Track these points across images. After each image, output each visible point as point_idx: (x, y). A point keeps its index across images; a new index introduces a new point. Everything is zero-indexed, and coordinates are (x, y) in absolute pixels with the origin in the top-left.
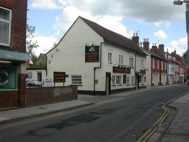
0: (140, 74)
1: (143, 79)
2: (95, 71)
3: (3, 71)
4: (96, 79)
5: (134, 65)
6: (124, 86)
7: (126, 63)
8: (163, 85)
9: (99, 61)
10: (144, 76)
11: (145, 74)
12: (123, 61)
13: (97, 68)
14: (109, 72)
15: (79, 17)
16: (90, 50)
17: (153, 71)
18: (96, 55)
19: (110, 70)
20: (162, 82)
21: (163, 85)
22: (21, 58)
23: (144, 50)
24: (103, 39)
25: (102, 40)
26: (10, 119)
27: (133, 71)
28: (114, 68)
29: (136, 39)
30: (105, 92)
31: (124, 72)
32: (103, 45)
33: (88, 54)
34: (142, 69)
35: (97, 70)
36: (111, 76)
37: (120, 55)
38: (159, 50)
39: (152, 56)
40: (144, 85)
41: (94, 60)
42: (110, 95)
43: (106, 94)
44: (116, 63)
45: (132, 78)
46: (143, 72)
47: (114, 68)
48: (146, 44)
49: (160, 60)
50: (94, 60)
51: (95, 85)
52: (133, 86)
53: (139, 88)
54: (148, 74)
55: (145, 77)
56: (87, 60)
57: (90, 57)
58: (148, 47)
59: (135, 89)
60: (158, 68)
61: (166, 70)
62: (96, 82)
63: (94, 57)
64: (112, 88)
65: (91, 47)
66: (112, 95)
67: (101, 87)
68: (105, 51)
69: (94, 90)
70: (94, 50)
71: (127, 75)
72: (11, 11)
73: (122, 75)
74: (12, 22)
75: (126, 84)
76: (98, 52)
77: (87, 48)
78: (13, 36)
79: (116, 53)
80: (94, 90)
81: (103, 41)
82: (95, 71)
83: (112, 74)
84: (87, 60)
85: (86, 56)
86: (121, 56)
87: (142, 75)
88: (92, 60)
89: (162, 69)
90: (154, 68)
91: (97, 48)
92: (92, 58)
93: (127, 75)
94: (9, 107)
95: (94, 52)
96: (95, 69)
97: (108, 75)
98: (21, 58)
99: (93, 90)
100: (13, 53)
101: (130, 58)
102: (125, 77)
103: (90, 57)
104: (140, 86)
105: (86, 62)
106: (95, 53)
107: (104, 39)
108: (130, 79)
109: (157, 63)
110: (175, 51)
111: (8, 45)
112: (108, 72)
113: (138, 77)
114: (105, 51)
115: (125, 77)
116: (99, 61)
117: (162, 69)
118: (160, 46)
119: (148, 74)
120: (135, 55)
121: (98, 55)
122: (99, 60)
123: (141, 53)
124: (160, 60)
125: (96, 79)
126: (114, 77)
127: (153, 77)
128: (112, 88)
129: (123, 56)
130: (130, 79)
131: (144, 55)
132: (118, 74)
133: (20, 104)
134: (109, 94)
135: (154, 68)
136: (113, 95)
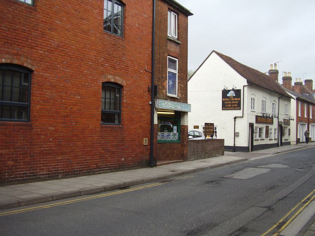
0: (283, 126)
1: (286, 131)
2: (235, 121)
3: (168, 123)
4: (236, 131)
5: (277, 112)
6: (267, 142)
7: (269, 111)
8: (312, 142)
9: (240, 109)
10: (288, 128)
11: (289, 125)
12: (266, 108)
13: (238, 117)
14: (252, 122)
15: (213, 51)
16: (228, 95)
17: (299, 120)
18: (236, 101)
19: (253, 121)
20: (310, 137)
21: (312, 142)
22: (186, 109)
23: (288, 92)
24: (246, 80)
25: (244, 82)
26: (108, 184)
27: (275, 121)
28: (257, 117)
29: (275, 73)
30: (278, 143)
31: (266, 123)
32: (246, 89)
33: (226, 99)
34: (286, 118)
35: (237, 120)
36: (254, 128)
37: (252, 98)
38: (305, 87)
39: (298, 99)
40: (288, 141)
41: (234, 107)
42: (252, 152)
43: (249, 151)
44: (259, 112)
45: (275, 130)
46: (287, 122)
47: (257, 117)
48: (287, 79)
49: (309, 103)
50: (234, 107)
51: (235, 138)
52: (276, 142)
53: (282, 144)
54: (293, 124)
55: (289, 129)
56: (225, 106)
57: (228, 104)
58: (290, 84)
59: (277, 145)
60: (306, 116)
61: (306, 116)
62: (236, 135)
63: (235, 104)
64: (255, 143)
65: (229, 91)
66: (254, 152)
67: (243, 141)
68: (247, 95)
69: (234, 144)
70: (234, 95)
71: (270, 126)
72: (177, 60)
73: (264, 126)
74: (179, 73)
75: (269, 138)
76: (240, 97)
77: (225, 93)
78: (180, 86)
79: (260, 96)
80: (234, 144)
81: (246, 84)
82: (235, 121)
83: (255, 125)
84: (225, 106)
85: (223, 102)
86: (264, 101)
87: (286, 126)
88: (232, 107)
89: (311, 117)
90: (300, 115)
91: (238, 92)
92: (232, 104)
93: (270, 126)
94: (174, 160)
95: (234, 97)
96: (235, 118)
97: (251, 125)
98: (186, 109)
99: (232, 145)
100: (180, 104)
101: (273, 104)
102: (267, 128)
103: (228, 104)
104: (283, 141)
105: (223, 109)
106: (236, 99)
107: (248, 82)
108: (273, 131)
109: (304, 109)
110: (191, 14)
111: (176, 96)
112: (250, 122)
113: (281, 129)
114: (247, 95)
115: (267, 128)
116: (240, 109)
117: (311, 117)
118: (306, 81)
119: (293, 124)
120: (279, 99)
121: (240, 101)
122: (241, 108)
123: (285, 96)
124: (309, 103)
125: (236, 131)
126: (256, 128)
127: (299, 129)
128: (255, 143)
129: (254, 99)
130: (273, 131)
131: (289, 98)
132: (260, 126)
133: (183, 158)
134: (252, 150)
135: (300, 115)
136: (260, 152)
